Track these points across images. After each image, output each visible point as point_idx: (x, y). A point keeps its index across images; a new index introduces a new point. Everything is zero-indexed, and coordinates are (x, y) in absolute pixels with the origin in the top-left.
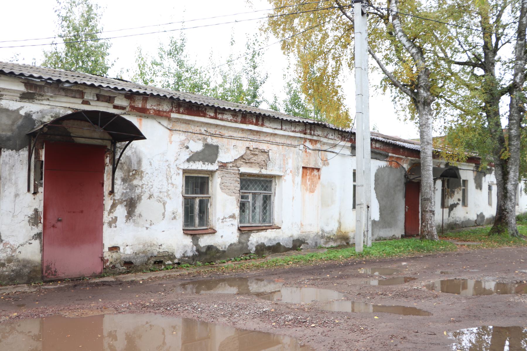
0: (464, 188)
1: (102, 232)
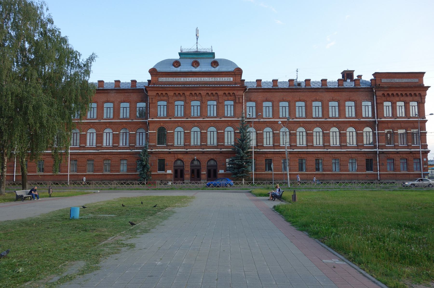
1: (156, 64)
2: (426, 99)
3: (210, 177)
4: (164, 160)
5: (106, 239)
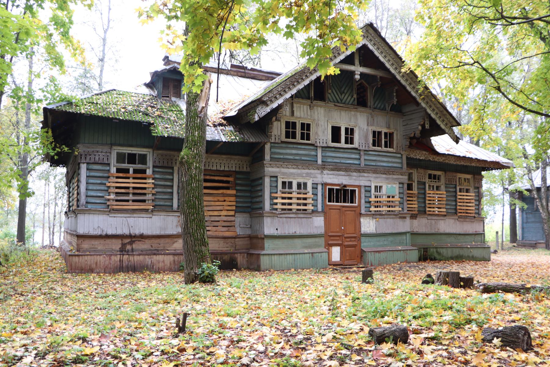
0: (131, 189)
2: (439, 136)
3: (329, 189)
4: (333, 141)
5: (298, 92)
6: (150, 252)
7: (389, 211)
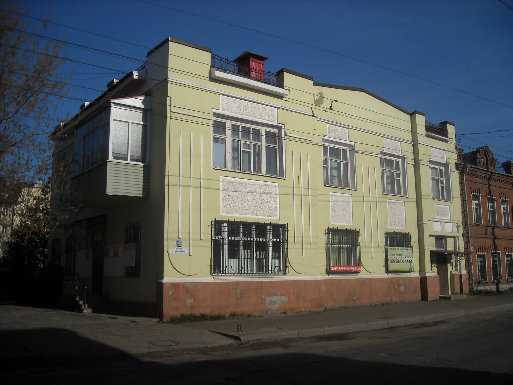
1: (249, 91)
6: (335, 253)
7: (391, 329)
